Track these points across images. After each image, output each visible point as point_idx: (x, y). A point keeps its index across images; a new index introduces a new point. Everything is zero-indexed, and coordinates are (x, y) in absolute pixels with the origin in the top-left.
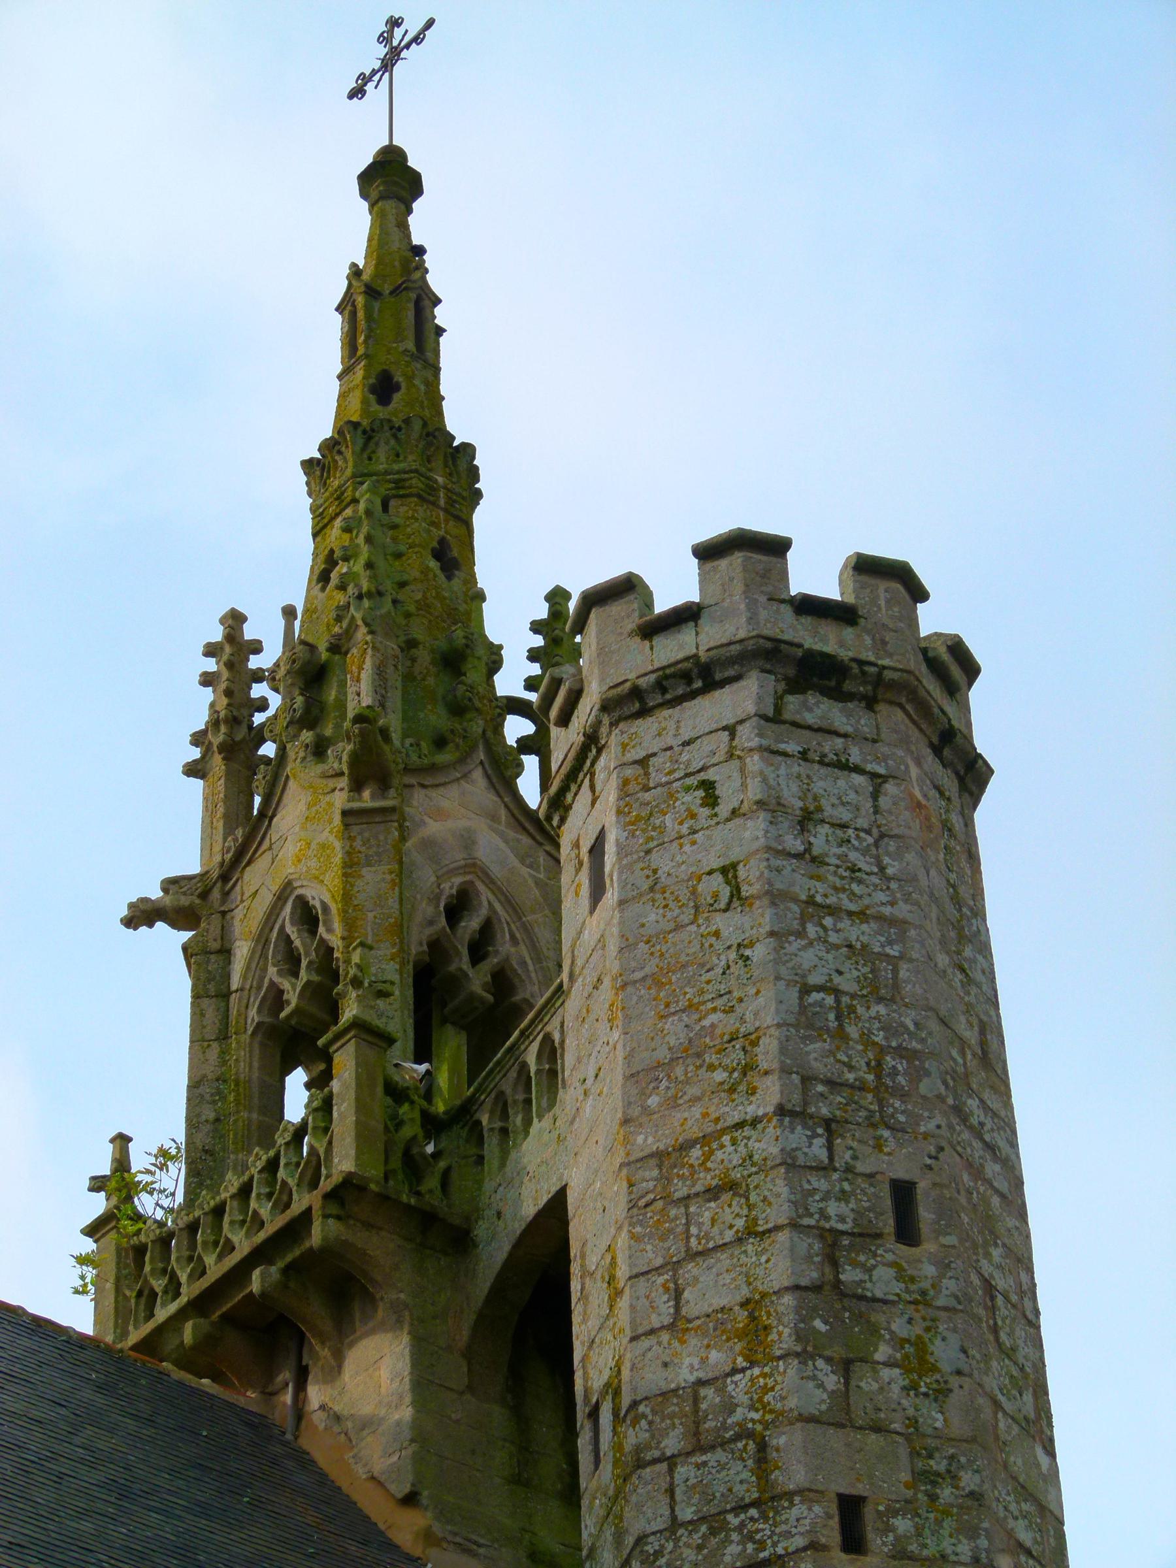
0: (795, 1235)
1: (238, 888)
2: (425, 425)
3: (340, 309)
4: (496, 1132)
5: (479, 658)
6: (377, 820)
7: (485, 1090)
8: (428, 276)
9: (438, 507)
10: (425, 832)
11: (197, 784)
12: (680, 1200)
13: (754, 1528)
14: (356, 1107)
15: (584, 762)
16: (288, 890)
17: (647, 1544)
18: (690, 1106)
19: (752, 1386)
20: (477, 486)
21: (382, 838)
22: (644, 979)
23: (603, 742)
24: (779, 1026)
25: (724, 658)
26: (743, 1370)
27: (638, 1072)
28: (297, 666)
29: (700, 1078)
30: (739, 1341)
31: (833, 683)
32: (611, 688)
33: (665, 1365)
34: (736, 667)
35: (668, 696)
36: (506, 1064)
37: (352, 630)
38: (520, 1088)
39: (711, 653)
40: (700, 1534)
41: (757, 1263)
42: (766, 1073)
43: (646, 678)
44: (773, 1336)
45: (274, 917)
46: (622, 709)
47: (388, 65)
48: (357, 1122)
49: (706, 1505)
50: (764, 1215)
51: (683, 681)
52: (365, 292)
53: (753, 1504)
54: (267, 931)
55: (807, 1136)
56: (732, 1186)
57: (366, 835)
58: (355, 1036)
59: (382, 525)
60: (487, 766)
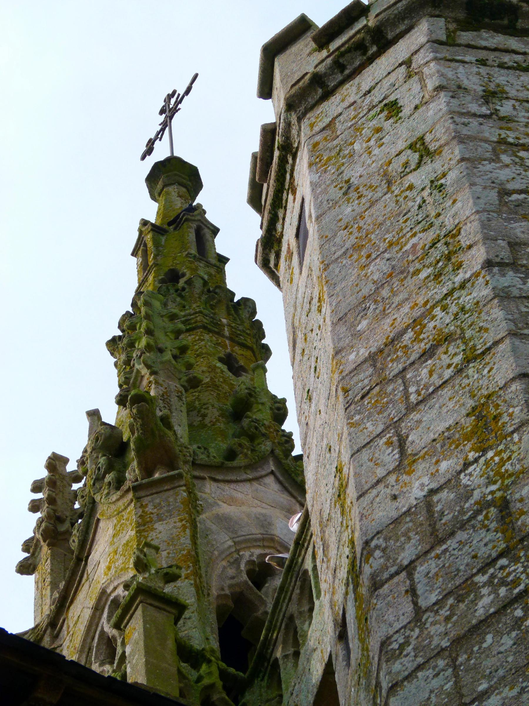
0: (517, 342)
1: (65, 628)
2: (205, 283)
3: (134, 253)
4: (291, 657)
5: (263, 404)
6: (166, 488)
7: (275, 626)
8: (206, 216)
9: (223, 336)
10: (216, 510)
11: (30, 580)
12: (396, 376)
13: (505, 574)
14: (146, 652)
15: (285, 178)
16: (104, 599)
17: (391, 643)
18: (399, 309)
19: (487, 468)
20: (263, 341)
21: (171, 500)
22: (345, 253)
23: (296, 145)
24: (477, 212)
25: (393, 16)
26: (476, 460)
27: (346, 314)
28: (100, 443)
29: (405, 286)
30: (468, 442)
31: (506, 22)
32: (293, 85)
33: (395, 497)
34: (406, 22)
35: (347, 72)
36: (288, 588)
37: (138, 382)
38: (305, 602)
39: (380, 18)
40: (448, 607)
41: (480, 377)
42: (470, 247)
43: (324, 64)
44: (505, 418)
45: (94, 627)
46: (306, 100)
47: (166, 125)
48: (147, 663)
49: (449, 582)
50: (481, 341)
51: (359, 53)
52: (152, 230)
53: (501, 555)
54: (89, 640)
55: (520, 278)
56: (448, 338)
57: (157, 501)
58: (141, 602)
59: (162, 316)
60: (278, 474)
